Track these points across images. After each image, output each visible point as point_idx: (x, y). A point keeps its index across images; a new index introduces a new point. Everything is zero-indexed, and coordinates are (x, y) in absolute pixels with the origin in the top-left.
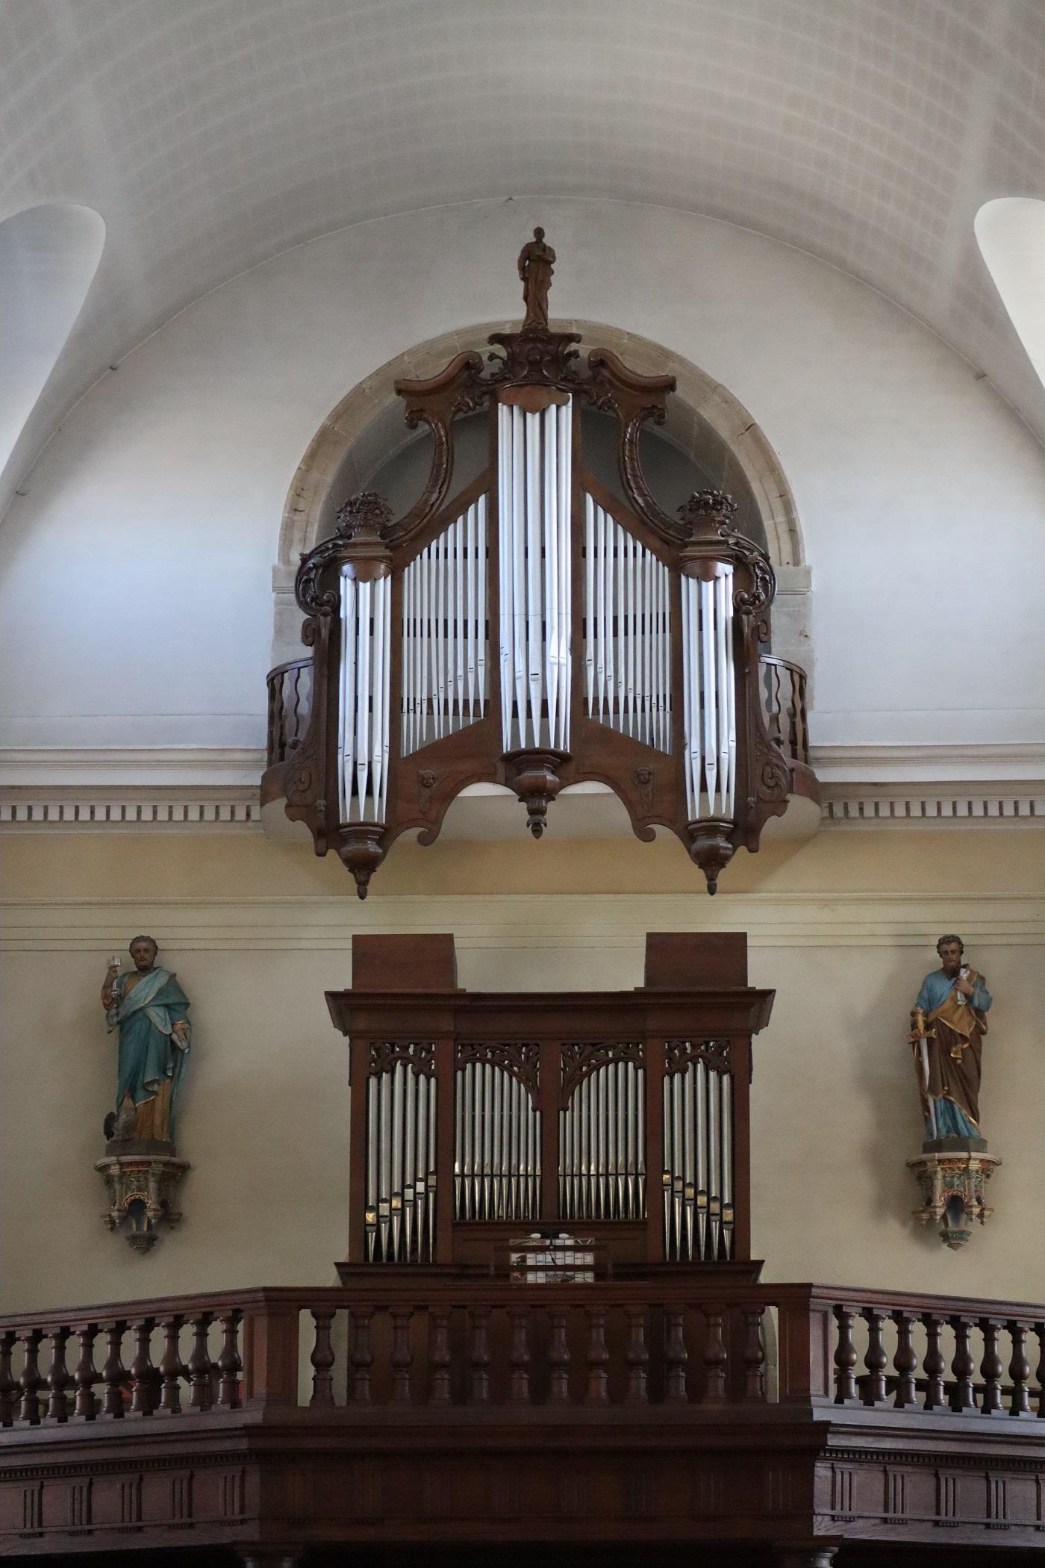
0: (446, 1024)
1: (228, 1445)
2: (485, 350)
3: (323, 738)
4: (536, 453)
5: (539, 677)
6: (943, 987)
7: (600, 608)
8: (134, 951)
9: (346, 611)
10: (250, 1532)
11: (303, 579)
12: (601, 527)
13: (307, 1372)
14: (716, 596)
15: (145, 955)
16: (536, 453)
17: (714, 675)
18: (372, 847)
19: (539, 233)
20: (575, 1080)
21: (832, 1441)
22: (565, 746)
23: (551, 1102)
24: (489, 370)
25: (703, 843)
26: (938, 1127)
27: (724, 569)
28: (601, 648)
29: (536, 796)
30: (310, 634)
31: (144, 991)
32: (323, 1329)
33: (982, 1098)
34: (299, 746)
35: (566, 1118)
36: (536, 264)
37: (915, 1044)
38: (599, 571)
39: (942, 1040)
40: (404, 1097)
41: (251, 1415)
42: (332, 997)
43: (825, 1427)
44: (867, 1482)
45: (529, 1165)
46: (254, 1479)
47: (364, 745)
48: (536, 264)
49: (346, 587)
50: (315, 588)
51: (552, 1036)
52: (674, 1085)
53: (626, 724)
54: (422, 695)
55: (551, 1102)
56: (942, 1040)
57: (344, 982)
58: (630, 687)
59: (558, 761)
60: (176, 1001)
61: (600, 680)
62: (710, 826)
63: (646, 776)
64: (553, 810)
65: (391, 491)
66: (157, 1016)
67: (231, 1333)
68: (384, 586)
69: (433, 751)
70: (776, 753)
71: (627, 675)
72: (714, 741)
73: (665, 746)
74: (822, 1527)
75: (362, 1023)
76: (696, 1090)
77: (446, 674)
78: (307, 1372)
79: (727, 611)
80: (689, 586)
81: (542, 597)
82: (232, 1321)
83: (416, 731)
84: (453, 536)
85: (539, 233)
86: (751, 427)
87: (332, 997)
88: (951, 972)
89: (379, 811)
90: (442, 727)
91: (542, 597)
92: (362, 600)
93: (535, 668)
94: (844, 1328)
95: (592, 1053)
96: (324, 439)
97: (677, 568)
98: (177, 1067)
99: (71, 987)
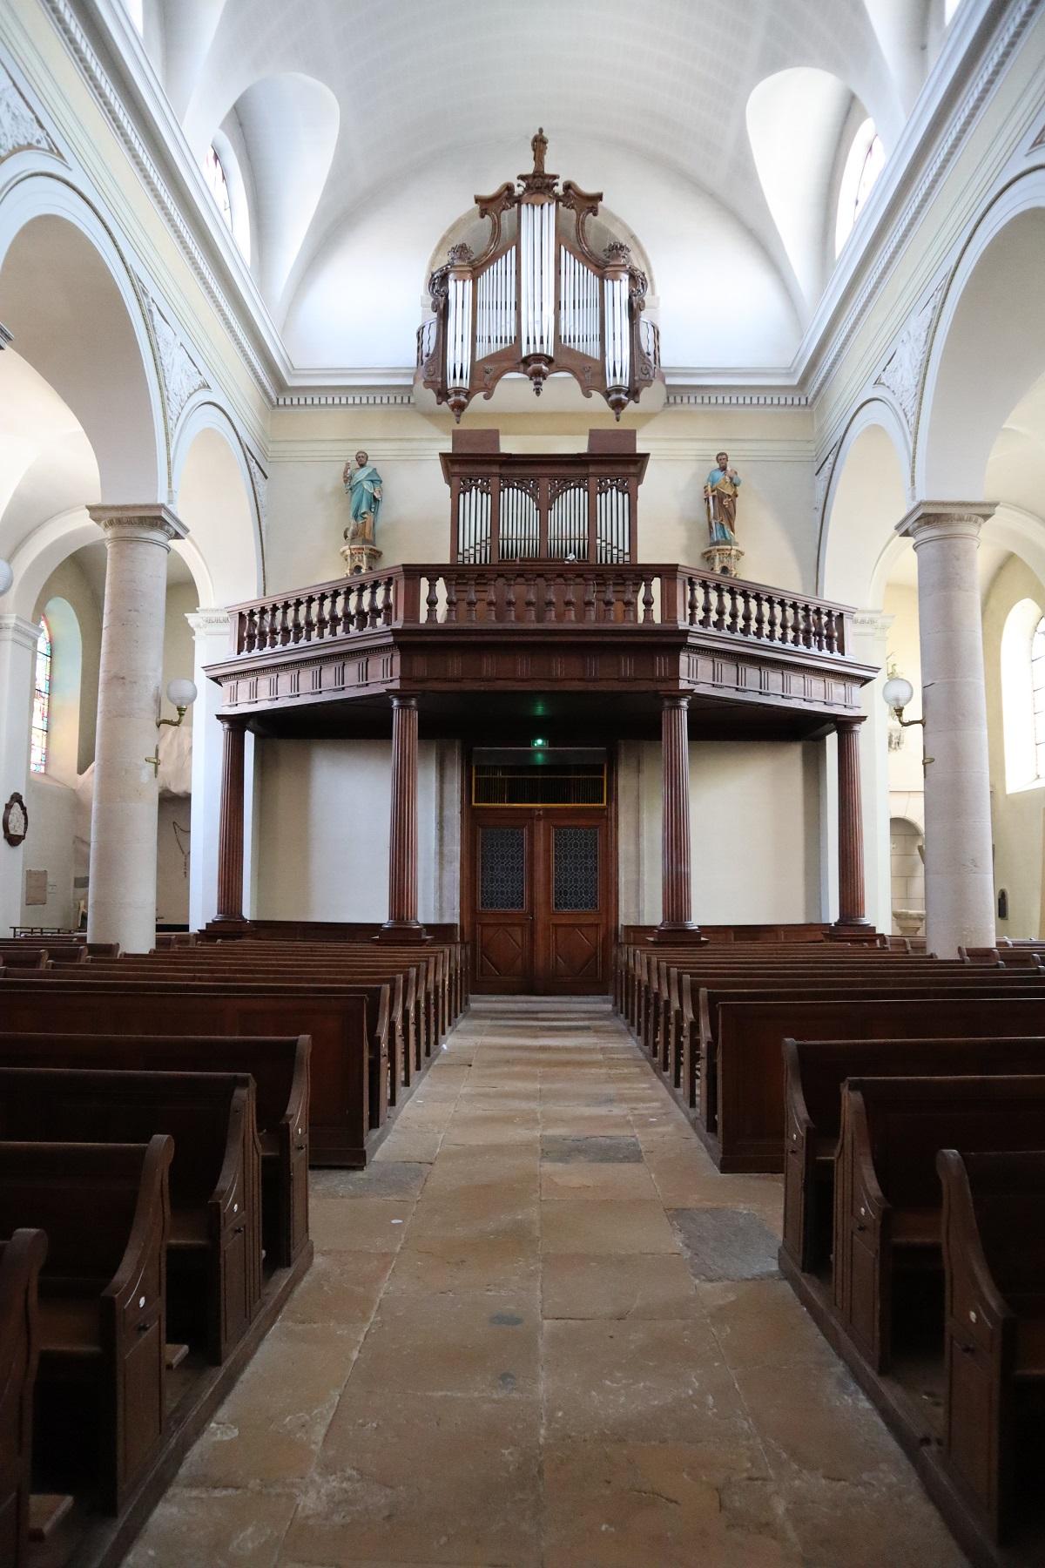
0: (495, 469)
1: (384, 641)
2: (515, 182)
3: (479, 864)
4: (538, 226)
5: (538, 329)
6: (720, 475)
7: (567, 297)
8: (358, 458)
9: (451, 297)
10: (396, 685)
11: (432, 283)
12: (568, 261)
13: (424, 607)
14: (620, 289)
15: (362, 461)
16: (538, 226)
17: (619, 323)
18: (463, 399)
19: (541, 130)
20: (556, 496)
21: (690, 640)
22: (551, 353)
23: (544, 507)
24: (518, 191)
25: (614, 397)
26: (717, 535)
27: (625, 277)
28: (567, 315)
29: (537, 376)
30: (435, 308)
31: (361, 474)
32: (432, 586)
33: (736, 526)
34: (434, 363)
35: (551, 514)
36: (539, 144)
37: (707, 500)
38: (567, 281)
39: (720, 497)
40: (475, 503)
41: (398, 624)
42: (443, 455)
43: (686, 633)
44: (705, 666)
45: (534, 531)
46: (397, 660)
47: (458, 356)
48: (539, 144)
49: (451, 284)
50: (439, 282)
51: (544, 474)
52: (601, 499)
53: (580, 347)
54: (486, 334)
55: (544, 507)
56: (720, 497)
57: (448, 448)
58: (579, 332)
59: (549, 361)
60: (375, 480)
61: (567, 328)
62: (618, 389)
63: (590, 373)
64: (545, 385)
65: (471, 258)
66: (367, 485)
67: (387, 590)
68: (469, 284)
69: (491, 359)
70: (643, 366)
71: (578, 326)
72: (618, 355)
73: (596, 355)
74: (683, 685)
75: (456, 469)
76: (612, 501)
77: (495, 328)
78: (424, 607)
79: (626, 297)
80: (608, 284)
81: (538, 292)
82: (388, 584)
83: (483, 351)
84: (501, 262)
85: (541, 130)
86: (633, 237)
87: (443, 455)
88: (723, 469)
89: (466, 384)
90: (495, 348)
91: (538, 292)
92: (458, 290)
93: (538, 318)
94: (692, 590)
95: (565, 484)
96: (444, 240)
97: (602, 278)
98: (377, 508)
99: (331, 477)
